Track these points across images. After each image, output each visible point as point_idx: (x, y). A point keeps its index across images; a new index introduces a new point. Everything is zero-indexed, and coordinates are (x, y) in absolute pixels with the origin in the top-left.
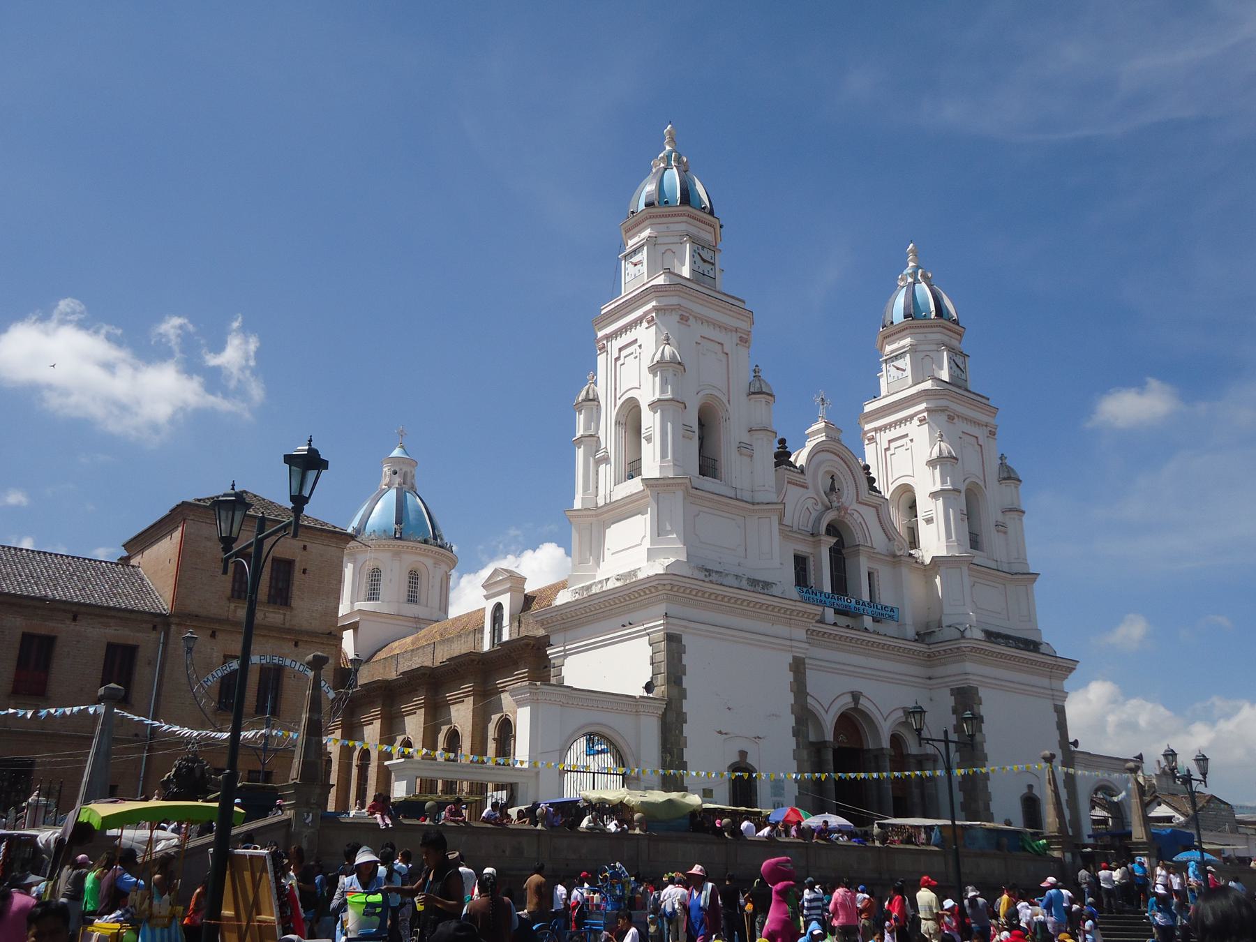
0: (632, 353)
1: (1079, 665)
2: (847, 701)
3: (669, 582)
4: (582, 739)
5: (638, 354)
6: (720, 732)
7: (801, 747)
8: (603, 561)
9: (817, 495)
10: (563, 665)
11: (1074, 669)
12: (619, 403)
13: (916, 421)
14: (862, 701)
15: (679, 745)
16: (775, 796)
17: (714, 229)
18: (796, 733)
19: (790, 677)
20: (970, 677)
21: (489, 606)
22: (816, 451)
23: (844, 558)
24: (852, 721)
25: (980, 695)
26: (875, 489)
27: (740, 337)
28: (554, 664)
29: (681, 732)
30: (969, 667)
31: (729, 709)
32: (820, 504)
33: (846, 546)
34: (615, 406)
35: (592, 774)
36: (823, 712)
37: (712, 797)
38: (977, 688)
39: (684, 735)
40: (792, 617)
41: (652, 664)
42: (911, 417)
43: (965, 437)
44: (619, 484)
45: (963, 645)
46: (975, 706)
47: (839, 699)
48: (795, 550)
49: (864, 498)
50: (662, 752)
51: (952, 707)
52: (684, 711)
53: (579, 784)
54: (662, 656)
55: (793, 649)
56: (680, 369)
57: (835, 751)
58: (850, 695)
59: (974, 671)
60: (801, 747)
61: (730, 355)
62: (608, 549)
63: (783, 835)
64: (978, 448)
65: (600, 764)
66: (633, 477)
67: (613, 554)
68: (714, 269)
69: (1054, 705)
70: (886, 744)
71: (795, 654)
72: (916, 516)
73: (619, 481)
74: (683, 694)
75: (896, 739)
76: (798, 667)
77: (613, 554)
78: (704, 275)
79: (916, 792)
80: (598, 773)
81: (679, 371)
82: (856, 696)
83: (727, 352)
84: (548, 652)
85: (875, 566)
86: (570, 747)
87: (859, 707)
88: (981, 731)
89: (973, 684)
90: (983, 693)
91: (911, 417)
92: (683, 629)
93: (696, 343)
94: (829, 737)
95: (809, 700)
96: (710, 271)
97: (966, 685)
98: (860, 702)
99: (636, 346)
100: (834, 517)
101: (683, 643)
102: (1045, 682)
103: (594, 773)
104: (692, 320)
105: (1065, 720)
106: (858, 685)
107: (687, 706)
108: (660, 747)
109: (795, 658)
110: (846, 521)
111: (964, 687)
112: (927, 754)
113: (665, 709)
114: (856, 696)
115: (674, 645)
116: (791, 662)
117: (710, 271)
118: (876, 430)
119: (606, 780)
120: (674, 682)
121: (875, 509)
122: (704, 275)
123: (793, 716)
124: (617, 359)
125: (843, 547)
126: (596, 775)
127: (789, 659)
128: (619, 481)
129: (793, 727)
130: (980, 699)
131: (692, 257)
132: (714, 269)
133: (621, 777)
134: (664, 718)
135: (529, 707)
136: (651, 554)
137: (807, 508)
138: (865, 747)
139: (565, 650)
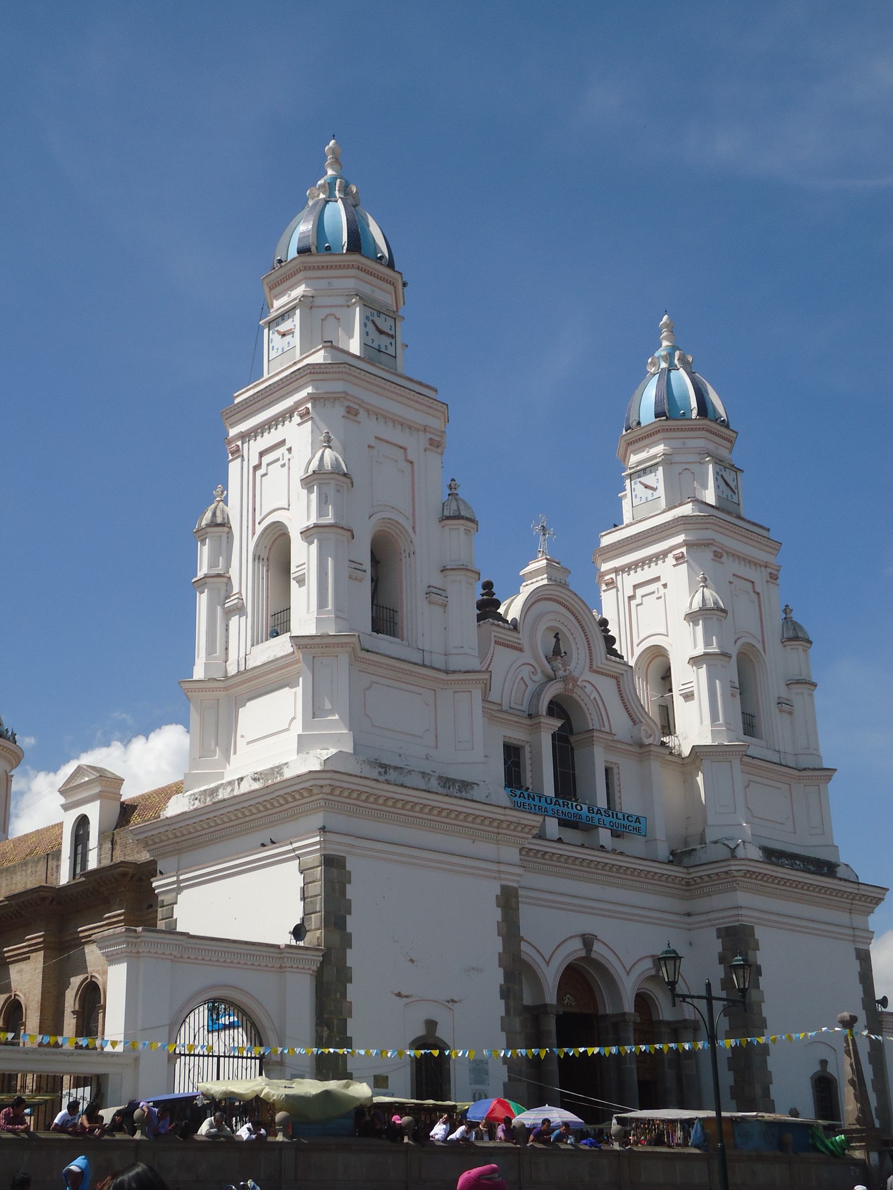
2: (575, 947)
3: (328, 782)
6: (399, 995)
7: (512, 1013)
8: (235, 753)
10: (176, 903)
12: (259, 529)
13: (670, 560)
14: (597, 947)
17: (395, 288)
18: (505, 993)
19: (497, 914)
20: (743, 912)
21: (69, 820)
23: (572, 749)
25: (756, 937)
26: (614, 653)
28: (163, 901)
30: (742, 898)
31: (412, 961)
34: (254, 534)
35: (215, 1059)
36: (543, 964)
37: (387, 1087)
39: (348, 999)
40: (501, 831)
41: (304, 898)
42: (665, 554)
43: (737, 581)
45: (733, 868)
48: (505, 736)
49: (600, 665)
50: (317, 1025)
53: (196, 1073)
54: (317, 888)
60: (512, 1013)
61: (416, 465)
62: (242, 736)
63: (486, 1138)
66: (278, 635)
67: (248, 743)
70: (629, 1007)
72: (671, 690)
77: (248, 743)
78: (380, 351)
80: (225, 1057)
82: (588, 941)
84: (154, 885)
91: (665, 554)
94: (551, 998)
95: (524, 947)
96: (389, 346)
97: (737, 924)
99: (283, 450)
102: (843, 918)
103: (219, 1057)
104: (362, 414)
109: (504, 888)
110: (574, 695)
114: (588, 941)
117: (389, 346)
118: (616, 571)
121: (614, 681)
122: (380, 351)
124: (257, 468)
125: (572, 733)
126: (222, 1059)
133: (258, 1061)
134: (319, 976)
135: (126, 964)
138: (601, 1012)
139: (178, 882)
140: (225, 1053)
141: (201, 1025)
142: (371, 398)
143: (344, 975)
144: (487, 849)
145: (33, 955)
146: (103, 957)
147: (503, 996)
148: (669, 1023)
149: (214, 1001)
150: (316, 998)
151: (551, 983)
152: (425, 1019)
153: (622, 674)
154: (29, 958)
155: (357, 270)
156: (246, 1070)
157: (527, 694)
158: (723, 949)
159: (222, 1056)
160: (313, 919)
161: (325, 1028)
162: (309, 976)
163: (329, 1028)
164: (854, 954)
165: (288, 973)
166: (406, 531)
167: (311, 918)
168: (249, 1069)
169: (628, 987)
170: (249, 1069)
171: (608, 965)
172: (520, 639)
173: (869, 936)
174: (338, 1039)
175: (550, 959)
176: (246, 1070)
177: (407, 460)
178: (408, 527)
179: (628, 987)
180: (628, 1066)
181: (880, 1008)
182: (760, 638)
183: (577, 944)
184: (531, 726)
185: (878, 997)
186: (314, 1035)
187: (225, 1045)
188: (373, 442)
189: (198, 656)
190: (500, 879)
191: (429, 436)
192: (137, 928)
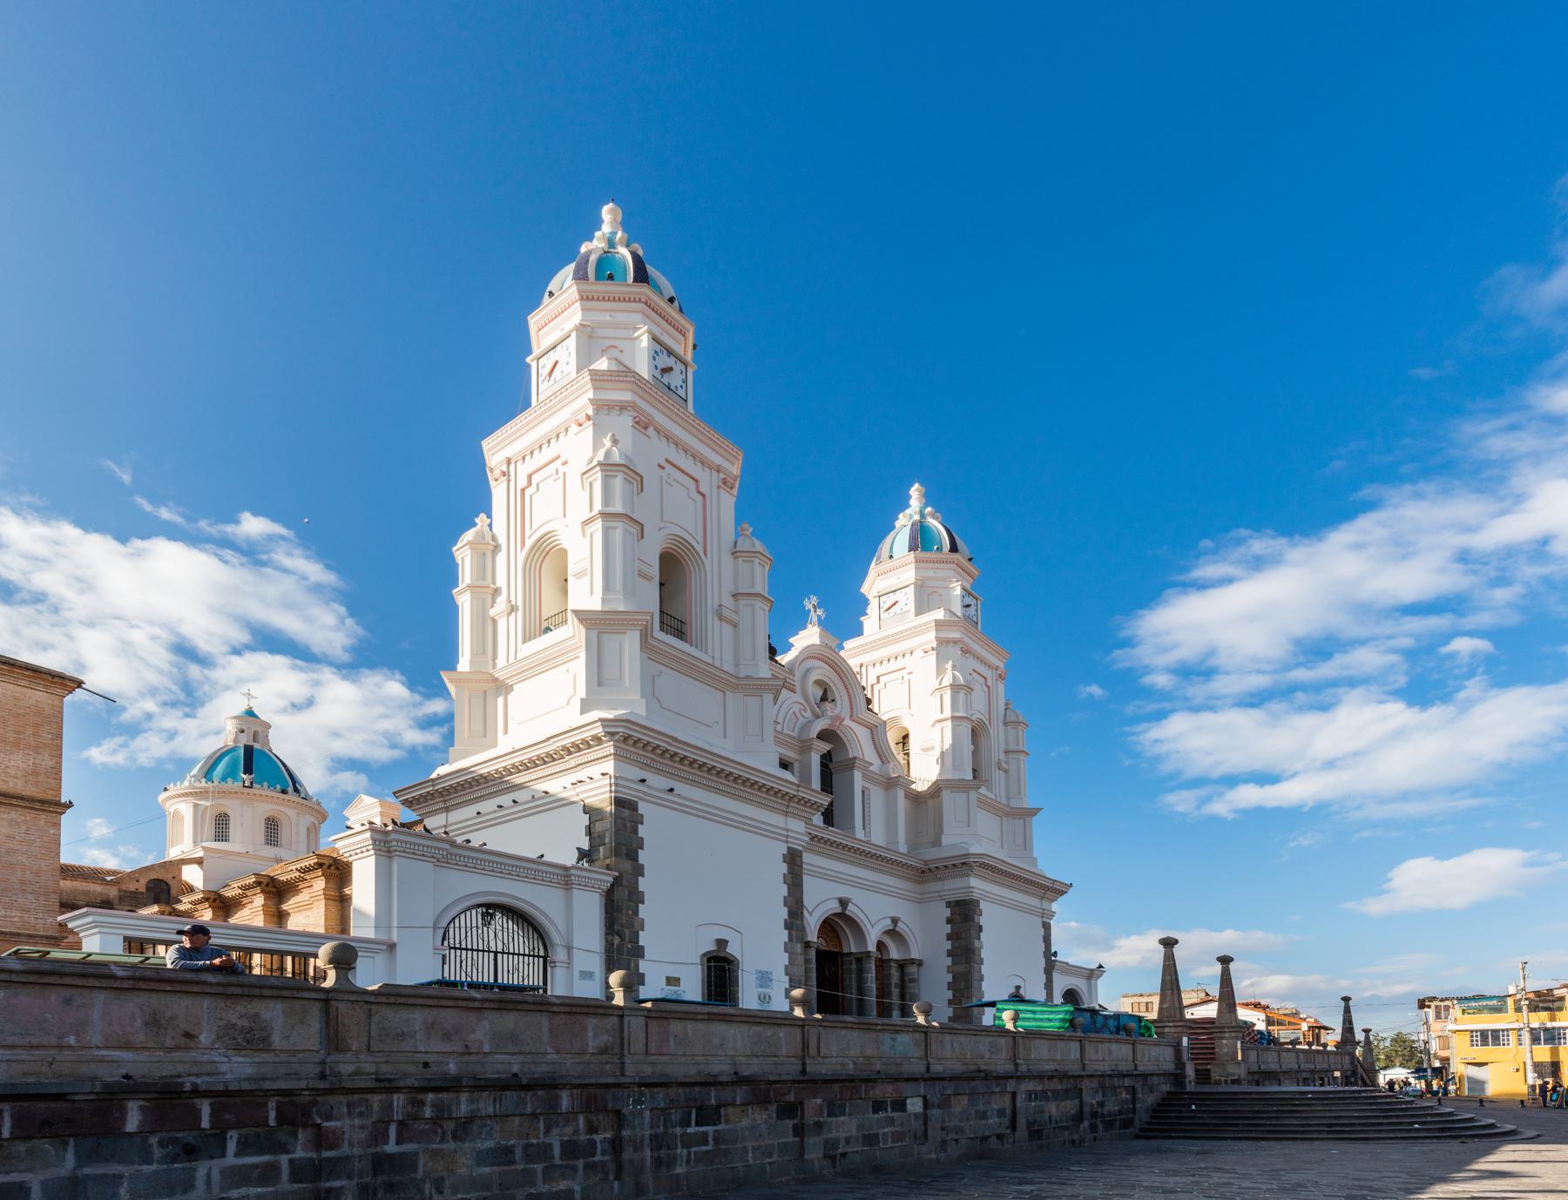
0: (552, 475)
1: (1071, 889)
2: (834, 907)
4: (474, 912)
5: (561, 475)
8: (506, 732)
9: (806, 701)
11: (1066, 892)
12: (529, 543)
14: (850, 907)
15: (633, 925)
16: (761, 987)
17: (686, 340)
19: (784, 868)
20: (975, 890)
22: (805, 656)
23: (831, 774)
24: (838, 924)
25: (981, 907)
27: (724, 479)
29: (636, 913)
30: (974, 882)
32: (808, 710)
33: (834, 761)
34: (523, 544)
35: (492, 955)
37: (679, 986)
38: (979, 901)
39: (640, 916)
43: (974, 674)
44: (530, 640)
46: (976, 916)
47: (818, 908)
49: (859, 716)
50: (606, 934)
51: (947, 918)
52: (640, 889)
53: (469, 963)
55: (785, 839)
56: (637, 481)
57: (819, 952)
58: (837, 901)
59: (978, 885)
63: (896, 1013)
64: (986, 689)
65: (506, 942)
67: (558, 457)
68: (684, 387)
69: (1043, 922)
70: (872, 947)
71: (790, 845)
73: (530, 635)
74: (639, 871)
75: (881, 946)
76: (793, 859)
77: (558, 457)
79: (840, 1000)
80: (503, 953)
81: (635, 483)
82: (844, 903)
83: (704, 492)
85: (867, 785)
86: (453, 919)
87: (847, 912)
88: (979, 939)
89: (975, 896)
90: (983, 905)
92: (641, 795)
93: (660, 466)
96: (679, 388)
98: (848, 908)
99: (557, 464)
100: (826, 727)
101: (640, 812)
102: (1035, 902)
103: (496, 953)
105: (1050, 935)
106: (844, 892)
107: (643, 884)
108: (604, 929)
109: (789, 849)
110: (839, 732)
111: (965, 900)
112: (913, 959)
113: (613, 885)
114: (844, 903)
115: (626, 812)
116: (786, 853)
119: (516, 975)
120: (626, 855)
121: (869, 731)
122: (669, 389)
123: (786, 909)
125: (831, 761)
126: (500, 956)
127: (783, 849)
128: (530, 635)
129: (785, 920)
130: (981, 911)
131: (652, 360)
132: (684, 387)
133: (541, 960)
136: (586, 706)
137: (794, 713)
138: (845, 951)
139: (434, 786)
140: (503, 949)
141: (474, 924)
142: (660, 419)
143: (637, 898)
144: (777, 819)
145: (316, 903)
146: (231, 727)
147: (786, 928)
148: (896, 961)
149: (488, 906)
150: (606, 913)
151: (812, 927)
152: (717, 937)
153: (876, 726)
154: (312, 908)
155: (644, 305)
156: (528, 965)
157: (798, 725)
158: (952, 914)
159: (500, 953)
160: (601, 851)
161: (616, 937)
162: (598, 895)
163: (620, 937)
164: (1041, 924)
165: (574, 890)
166: (697, 553)
167: (599, 850)
168: (531, 965)
169: (873, 936)
170: (531, 965)
171: (858, 921)
172: (794, 681)
173: (1052, 915)
174: (629, 946)
175: (813, 911)
176: (528, 965)
177: (699, 492)
178: (700, 549)
179: (873, 936)
180: (869, 985)
181: (1053, 958)
182: (987, 716)
183: (889, 922)
184: (801, 747)
185: (1053, 951)
186: (604, 943)
187: (503, 943)
188: (664, 463)
189: (462, 656)
190: (787, 842)
191: (722, 476)
192: (576, 1162)
